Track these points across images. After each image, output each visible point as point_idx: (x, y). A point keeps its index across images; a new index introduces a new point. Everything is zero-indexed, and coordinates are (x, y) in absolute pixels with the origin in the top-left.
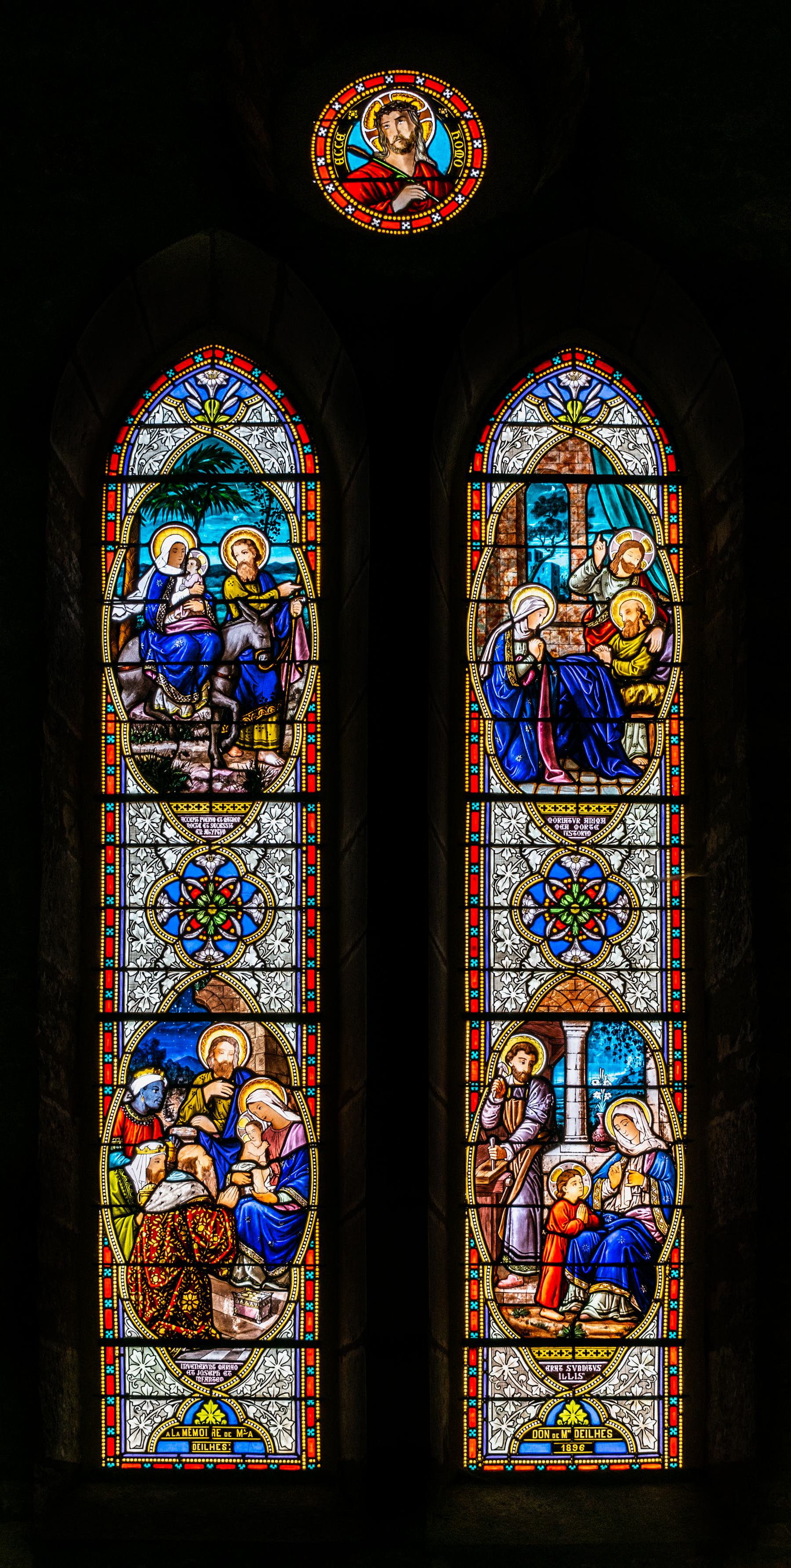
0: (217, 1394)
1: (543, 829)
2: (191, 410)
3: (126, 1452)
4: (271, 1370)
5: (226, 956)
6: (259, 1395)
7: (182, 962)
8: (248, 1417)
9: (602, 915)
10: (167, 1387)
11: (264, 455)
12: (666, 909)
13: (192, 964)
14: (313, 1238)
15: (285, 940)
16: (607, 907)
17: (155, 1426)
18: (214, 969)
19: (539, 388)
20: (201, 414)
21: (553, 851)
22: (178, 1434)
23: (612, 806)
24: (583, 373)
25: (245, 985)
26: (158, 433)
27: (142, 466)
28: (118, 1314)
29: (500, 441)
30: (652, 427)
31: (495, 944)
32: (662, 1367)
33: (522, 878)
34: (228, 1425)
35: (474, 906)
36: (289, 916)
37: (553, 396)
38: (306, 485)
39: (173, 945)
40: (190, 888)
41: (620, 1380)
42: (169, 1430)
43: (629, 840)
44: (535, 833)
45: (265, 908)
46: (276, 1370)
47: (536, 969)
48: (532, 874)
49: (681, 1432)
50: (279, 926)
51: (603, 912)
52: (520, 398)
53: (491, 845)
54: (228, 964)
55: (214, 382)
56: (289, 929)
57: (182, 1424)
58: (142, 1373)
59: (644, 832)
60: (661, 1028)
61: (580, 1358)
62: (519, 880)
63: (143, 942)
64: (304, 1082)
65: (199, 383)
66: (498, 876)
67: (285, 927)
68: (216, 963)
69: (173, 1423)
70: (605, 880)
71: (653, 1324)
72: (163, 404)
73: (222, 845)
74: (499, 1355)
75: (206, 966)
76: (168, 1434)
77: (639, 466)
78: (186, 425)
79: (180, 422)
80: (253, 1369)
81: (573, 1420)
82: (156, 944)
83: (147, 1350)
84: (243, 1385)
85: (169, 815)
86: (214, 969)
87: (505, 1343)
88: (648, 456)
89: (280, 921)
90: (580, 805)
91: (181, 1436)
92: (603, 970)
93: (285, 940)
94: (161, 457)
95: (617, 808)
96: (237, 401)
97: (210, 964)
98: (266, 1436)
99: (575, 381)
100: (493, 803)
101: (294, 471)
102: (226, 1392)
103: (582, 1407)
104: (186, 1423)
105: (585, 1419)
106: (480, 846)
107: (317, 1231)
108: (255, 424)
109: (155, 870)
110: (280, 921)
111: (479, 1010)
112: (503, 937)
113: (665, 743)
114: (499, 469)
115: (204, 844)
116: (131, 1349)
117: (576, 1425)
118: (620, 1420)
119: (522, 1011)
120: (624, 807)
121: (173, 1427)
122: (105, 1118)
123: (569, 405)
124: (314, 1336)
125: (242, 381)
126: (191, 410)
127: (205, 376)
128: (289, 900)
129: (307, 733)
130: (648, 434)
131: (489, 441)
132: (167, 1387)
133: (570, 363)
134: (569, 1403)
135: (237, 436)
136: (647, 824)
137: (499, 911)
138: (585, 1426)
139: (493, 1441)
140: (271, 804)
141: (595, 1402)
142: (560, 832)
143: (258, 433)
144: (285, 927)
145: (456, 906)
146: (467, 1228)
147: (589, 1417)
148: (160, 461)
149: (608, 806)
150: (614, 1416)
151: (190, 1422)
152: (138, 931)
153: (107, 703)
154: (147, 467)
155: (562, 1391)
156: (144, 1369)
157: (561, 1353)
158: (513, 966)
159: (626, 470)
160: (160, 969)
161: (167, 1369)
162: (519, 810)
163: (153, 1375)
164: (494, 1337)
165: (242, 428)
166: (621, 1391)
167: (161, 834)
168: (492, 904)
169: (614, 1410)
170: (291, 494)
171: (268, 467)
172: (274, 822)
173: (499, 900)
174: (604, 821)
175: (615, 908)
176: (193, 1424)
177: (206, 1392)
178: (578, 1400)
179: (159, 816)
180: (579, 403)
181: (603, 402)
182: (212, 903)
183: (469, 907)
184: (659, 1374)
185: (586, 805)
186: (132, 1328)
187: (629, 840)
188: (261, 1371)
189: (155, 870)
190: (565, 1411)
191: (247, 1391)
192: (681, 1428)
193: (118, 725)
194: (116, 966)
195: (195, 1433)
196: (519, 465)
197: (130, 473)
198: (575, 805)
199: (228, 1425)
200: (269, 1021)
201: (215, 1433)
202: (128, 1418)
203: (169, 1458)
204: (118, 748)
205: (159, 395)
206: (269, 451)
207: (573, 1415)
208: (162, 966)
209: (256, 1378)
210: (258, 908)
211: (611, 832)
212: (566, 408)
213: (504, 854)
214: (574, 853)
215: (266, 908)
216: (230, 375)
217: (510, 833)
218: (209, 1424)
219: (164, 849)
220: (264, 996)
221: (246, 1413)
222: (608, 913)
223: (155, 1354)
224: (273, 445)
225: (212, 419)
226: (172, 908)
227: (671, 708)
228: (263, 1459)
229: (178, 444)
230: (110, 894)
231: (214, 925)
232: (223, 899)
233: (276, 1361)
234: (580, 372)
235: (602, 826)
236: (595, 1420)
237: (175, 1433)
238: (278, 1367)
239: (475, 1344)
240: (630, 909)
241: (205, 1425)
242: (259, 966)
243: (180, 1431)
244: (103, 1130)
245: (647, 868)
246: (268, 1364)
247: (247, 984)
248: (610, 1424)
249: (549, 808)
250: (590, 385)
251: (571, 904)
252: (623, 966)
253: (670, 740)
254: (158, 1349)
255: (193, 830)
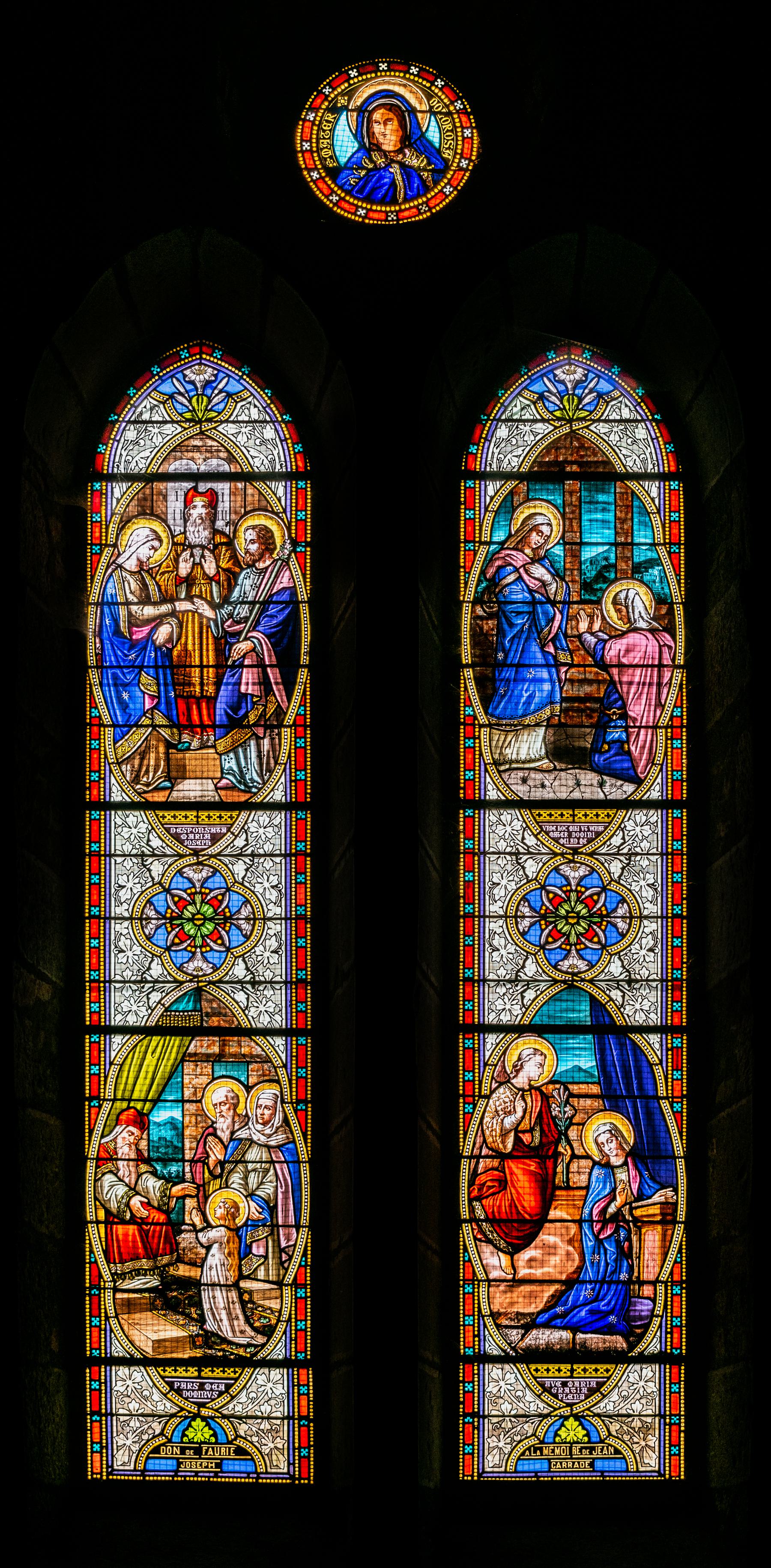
0: (204, 1412)
1: (539, 836)
2: (178, 406)
3: (288, 1473)
4: (263, 1388)
5: (215, 968)
6: (623, 1412)
7: (169, 974)
8: (610, 1434)
9: (601, 925)
10: (527, 1404)
11: (624, 451)
12: (667, 917)
13: (180, 977)
14: (680, 1251)
15: (651, 950)
16: (231, 918)
17: (514, 1444)
18: (202, 981)
19: (163, 385)
20: (560, 409)
21: (176, 861)
22: (538, 1453)
23: (610, 813)
24: (209, 366)
25: (233, 999)
26: (146, 429)
27: (500, 461)
28: (105, 1334)
29: (122, 440)
30: (650, 421)
31: (116, 955)
32: (291, 1385)
33: (518, 886)
34: (589, 1442)
35: (94, 917)
36: (278, 927)
37: (549, 391)
38: (297, 484)
39: (535, 955)
40: (176, 899)
41: (249, 1398)
42: (529, 1449)
43: (252, 848)
44: (531, 841)
45: (630, 917)
46: (268, 1388)
47: (156, 981)
48: (528, 882)
49: (682, 1450)
50: (268, 937)
51: (602, 920)
52: (144, 395)
53: (485, 853)
54: (215, 977)
55: (572, 377)
56: (655, 939)
57: (542, 1442)
58: (502, 1390)
59: (268, 839)
60: (284, 1043)
61: (206, 1376)
62: (515, 888)
63: (130, 954)
64: (294, 1097)
65: (187, 379)
66: (494, 883)
67: (650, 936)
68: (204, 975)
69: (533, 1441)
70: (604, 889)
71: (280, 1344)
72: (521, 399)
73: (211, 856)
74: (494, 1371)
75: (194, 978)
76: (527, 1453)
77: (266, 462)
78: (543, 420)
79: (168, 419)
80: (245, 1386)
81: (199, 1437)
82: (143, 956)
83: (507, 1367)
84: (606, 1401)
85: (156, 824)
86: (202, 981)
87: (503, 1359)
88: (276, 453)
89: (646, 930)
90: (200, 814)
91: (542, 1455)
92: (227, 982)
93: (651, 950)
94: (520, 452)
95: (238, 816)
96: (226, 397)
97: (197, 976)
98: (627, 1453)
99: (199, 375)
100: (113, 812)
101: (284, 470)
102: (217, 1410)
103: (581, 1424)
104: (546, 1440)
105: (584, 1436)
106: (474, 854)
107: (309, 1248)
108: (615, 421)
109: (141, 881)
110: (646, 930)
111: (474, 1022)
112: (124, 949)
113: (666, 748)
114: (494, 466)
115: (190, 855)
116: (491, 1366)
117: (575, 1443)
118: (249, 1438)
119: (143, 1024)
120: (244, 815)
121: (533, 1446)
122: (465, 1134)
123: (194, 400)
124: (306, 1355)
125: (229, 376)
126: (178, 406)
127: (192, 372)
128: (278, 910)
129: (296, 738)
130: (276, 430)
131: (288, 436)
132: (527, 1404)
133: (198, 357)
134: (194, 1420)
135: (225, 433)
136: (647, 830)
137: (120, 921)
138: (212, 1444)
139: (490, 1458)
140: (260, 813)
141: (596, 1421)
142: (556, 840)
143: (246, 430)
144: (650, 936)
145: (450, 916)
146: (461, 1243)
147: (215, 1435)
148: (518, 456)
149: (229, 814)
150: (614, 1433)
151: (551, 1440)
152: (123, 943)
153: (91, 707)
154: (133, 464)
155: (560, 1408)
156: (268, 1388)
157: (559, 1370)
158: (133, 978)
159: (625, 466)
160: (147, 982)
161: (528, 1385)
162: (140, 819)
163: (513, 1393)
164: (116, 1355)
165: (230, 425)
166: (252, 1410)
167: (148, 844)
168: (113, 915)
169: (614, 1427)
170: (654, 493)
171: (257, 462)
172: (261, 831)
173: (121, 910)
174: (601, 829)
175: (238, 919)
176: (555, 1442)
177: (566, 1411)
178: (577, 1417)
179: (146, 826)
180: (205, 398)
181: (600, 396)
182: (572, 912)
183: (89, 918)
184: (660, 1390)
185: (206, 814)
186: (120, 1349)
187: (252, 848)
188: (254, 1388)
189: (516, 879)
190: (563, 1428)
191: (610, 1407)
192: (682, 1447)
193: (102, 729)
194: (476, 978)
195: (557, 1451)
196: (515, 462)
197: (488, 469)
198: (571, 812)
199: (589, 1442)
200: (635, 1033)
201: (575, 1451)
202: (486, 1436)
203: (161, 1476)
204: (102, 753)
205: (145, 390)
206: (258, 448)
207: (572, 1433)
208: (149, 978)
209: (619, 1394)
210: (247, 919)
211: (609, 839)
212: (562, 403)
213: (125, 864)
214: (570, 861)
215: (141, 919)
216: (589, 371)
217: (505, 840)
218: (569, 1443)
219: (150, 860)
220: (253, 1009)
221: (608, 1430)
222: (608, 922)
223: (516, 1371)
224: (634, 442)
225: (571, 414)
226: (158, 919)
227: (673, 711)
228: (245, 1478)
229: (165, 441)
230: (469, 901)
231: (576, 933)
232: (211, 910)
233: (640, 1377)
234: (206, 365)
235: (598, 834)
236: (222, 1438)
237: (535, 1452)
238: (642, 1383)
239: (469, 1360)
240: (630, 917)
241: (565, 1443)
242: (248, 978)
243: (541, 1449)
244: (89, 1145)
245: (271, 878)
246: (260, 1382)
247: (236, 997)
248: (611, 1441)
249: (545, 815)
250: (586, 380)
251: (194, 915)
252: (622, 977)
253: (672, 744)
254: (518, 1365)
255: (556, 840)
